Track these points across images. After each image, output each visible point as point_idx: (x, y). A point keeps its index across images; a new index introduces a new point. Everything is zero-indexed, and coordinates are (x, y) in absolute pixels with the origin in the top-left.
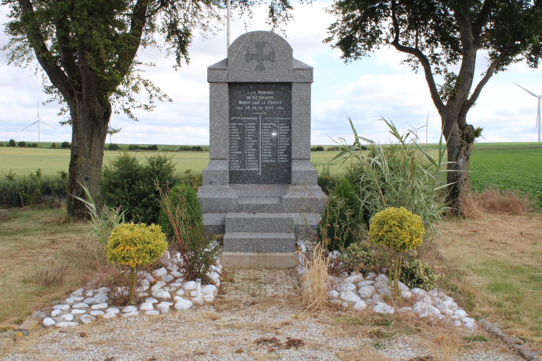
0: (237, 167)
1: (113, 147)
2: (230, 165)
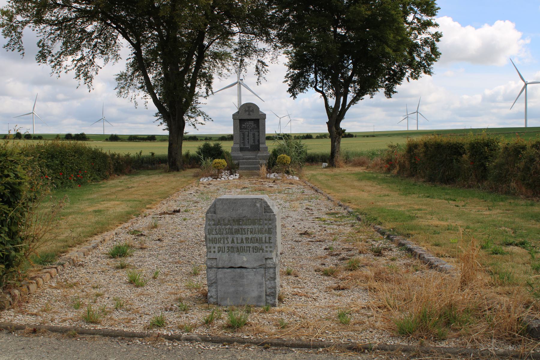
0: (242, 146)
1: (194, 138)
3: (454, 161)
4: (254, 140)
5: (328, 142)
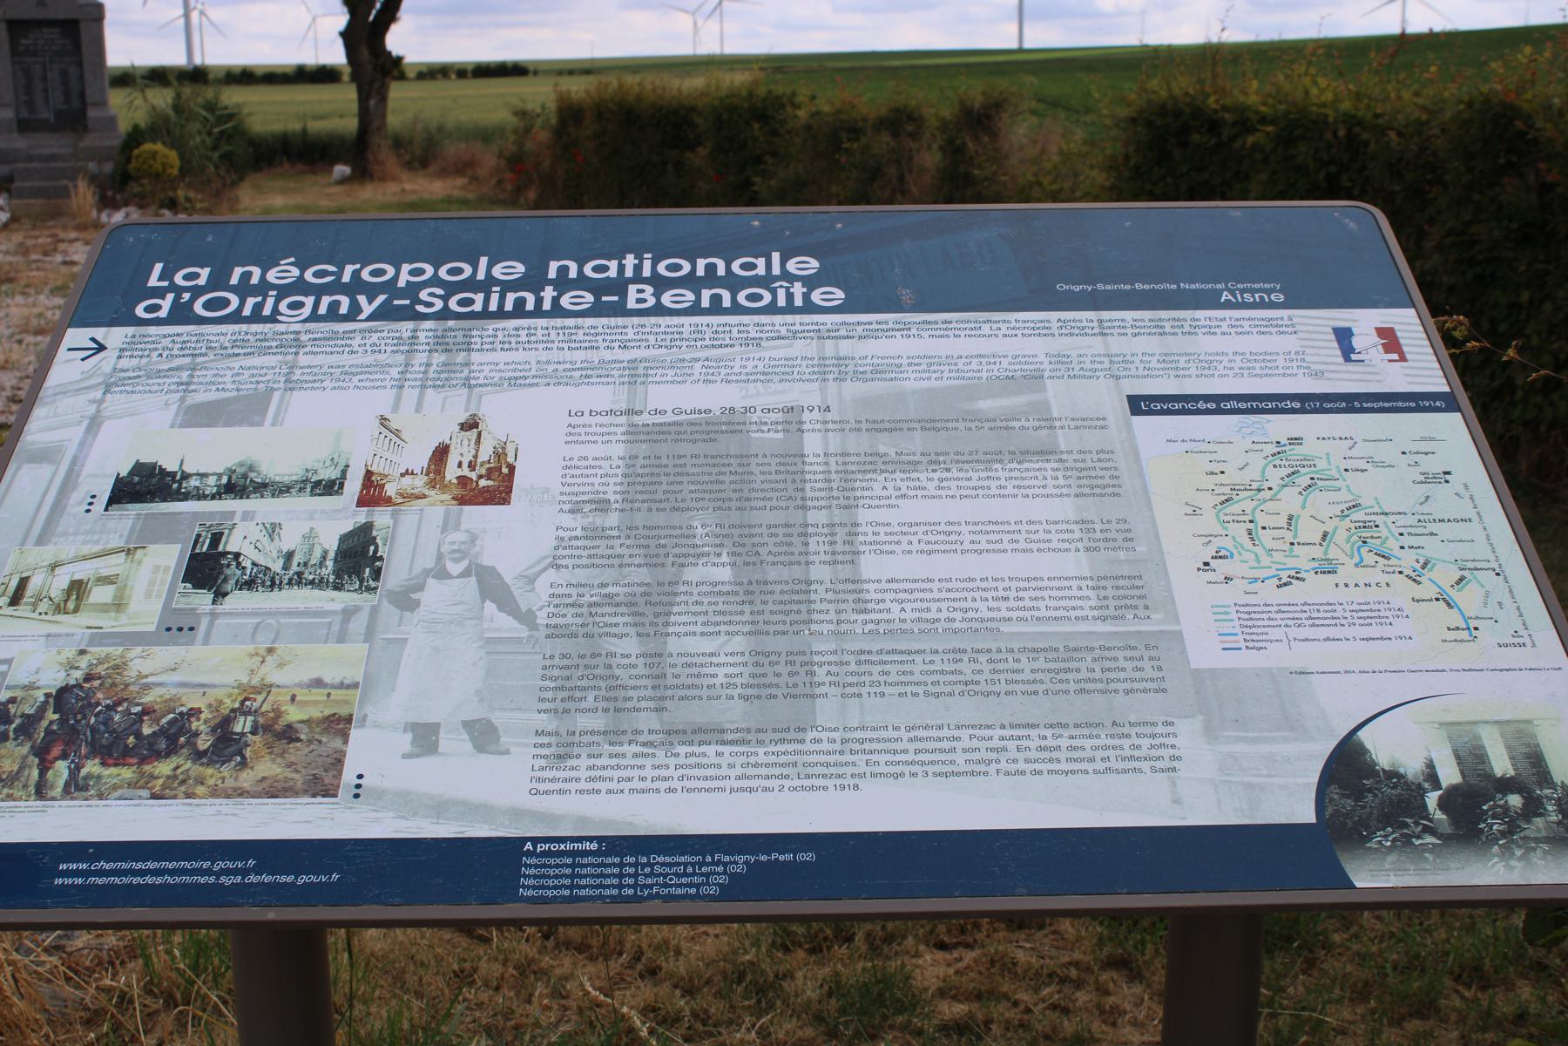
0: (25, 114)
2: (17, 112)
3: (670, 167)
4: (67, 94)
5: (345, 97)
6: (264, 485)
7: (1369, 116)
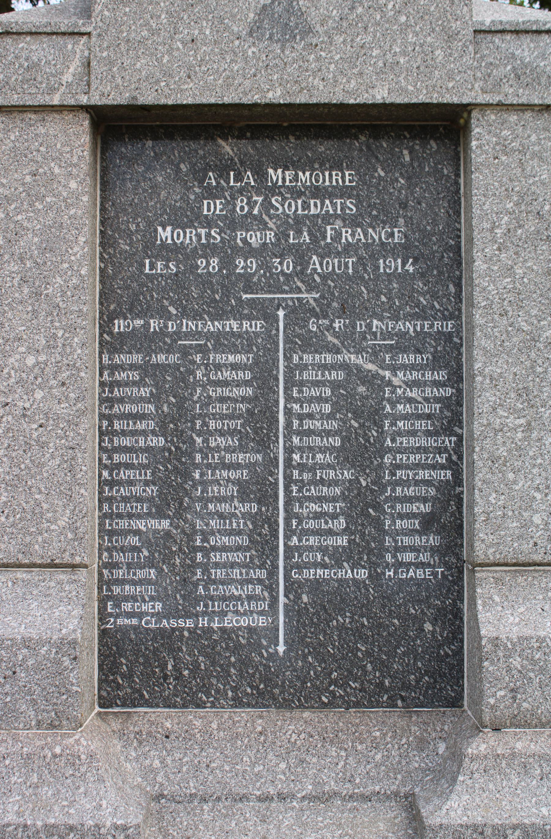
0: (146, 611)
2: (107, 596)
4: (364, 507)
6: (388, 797)
7: (49, 561)
